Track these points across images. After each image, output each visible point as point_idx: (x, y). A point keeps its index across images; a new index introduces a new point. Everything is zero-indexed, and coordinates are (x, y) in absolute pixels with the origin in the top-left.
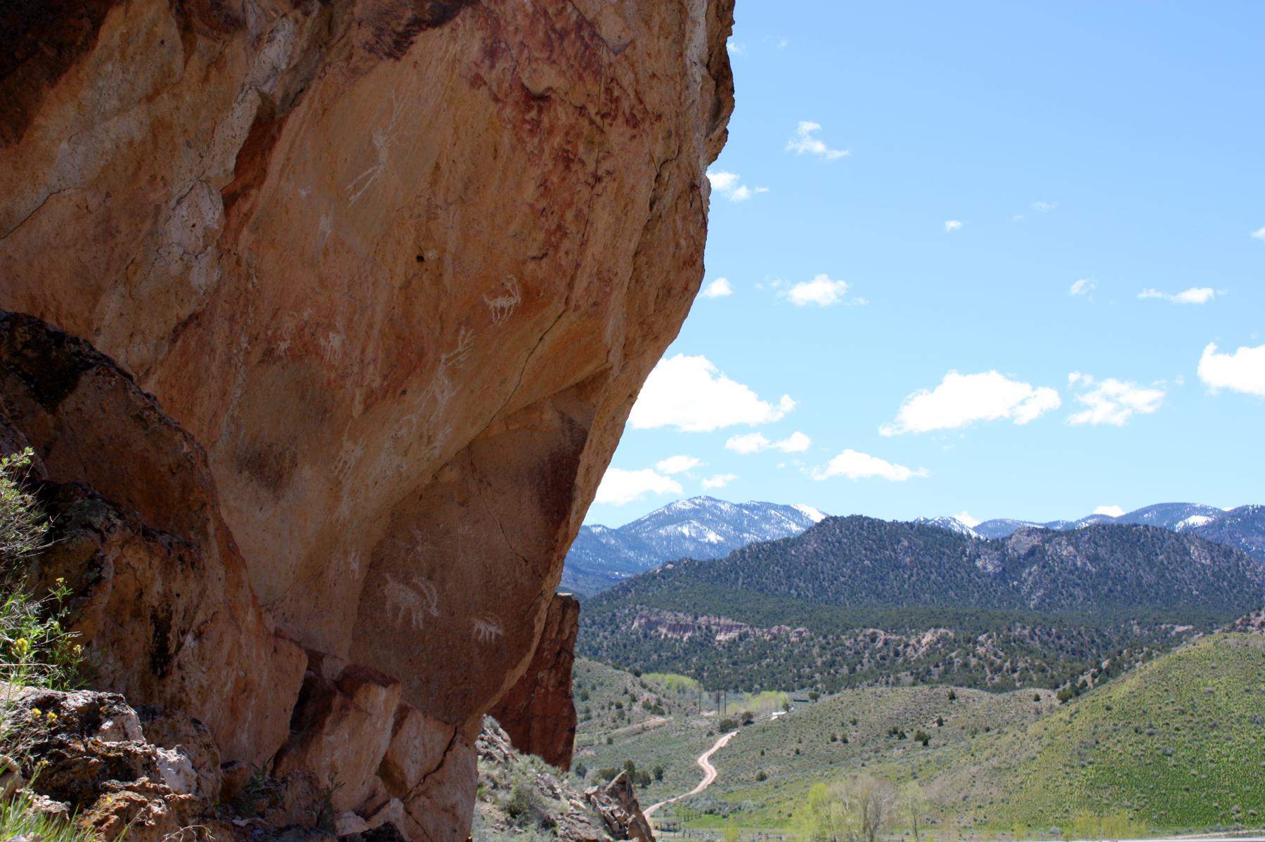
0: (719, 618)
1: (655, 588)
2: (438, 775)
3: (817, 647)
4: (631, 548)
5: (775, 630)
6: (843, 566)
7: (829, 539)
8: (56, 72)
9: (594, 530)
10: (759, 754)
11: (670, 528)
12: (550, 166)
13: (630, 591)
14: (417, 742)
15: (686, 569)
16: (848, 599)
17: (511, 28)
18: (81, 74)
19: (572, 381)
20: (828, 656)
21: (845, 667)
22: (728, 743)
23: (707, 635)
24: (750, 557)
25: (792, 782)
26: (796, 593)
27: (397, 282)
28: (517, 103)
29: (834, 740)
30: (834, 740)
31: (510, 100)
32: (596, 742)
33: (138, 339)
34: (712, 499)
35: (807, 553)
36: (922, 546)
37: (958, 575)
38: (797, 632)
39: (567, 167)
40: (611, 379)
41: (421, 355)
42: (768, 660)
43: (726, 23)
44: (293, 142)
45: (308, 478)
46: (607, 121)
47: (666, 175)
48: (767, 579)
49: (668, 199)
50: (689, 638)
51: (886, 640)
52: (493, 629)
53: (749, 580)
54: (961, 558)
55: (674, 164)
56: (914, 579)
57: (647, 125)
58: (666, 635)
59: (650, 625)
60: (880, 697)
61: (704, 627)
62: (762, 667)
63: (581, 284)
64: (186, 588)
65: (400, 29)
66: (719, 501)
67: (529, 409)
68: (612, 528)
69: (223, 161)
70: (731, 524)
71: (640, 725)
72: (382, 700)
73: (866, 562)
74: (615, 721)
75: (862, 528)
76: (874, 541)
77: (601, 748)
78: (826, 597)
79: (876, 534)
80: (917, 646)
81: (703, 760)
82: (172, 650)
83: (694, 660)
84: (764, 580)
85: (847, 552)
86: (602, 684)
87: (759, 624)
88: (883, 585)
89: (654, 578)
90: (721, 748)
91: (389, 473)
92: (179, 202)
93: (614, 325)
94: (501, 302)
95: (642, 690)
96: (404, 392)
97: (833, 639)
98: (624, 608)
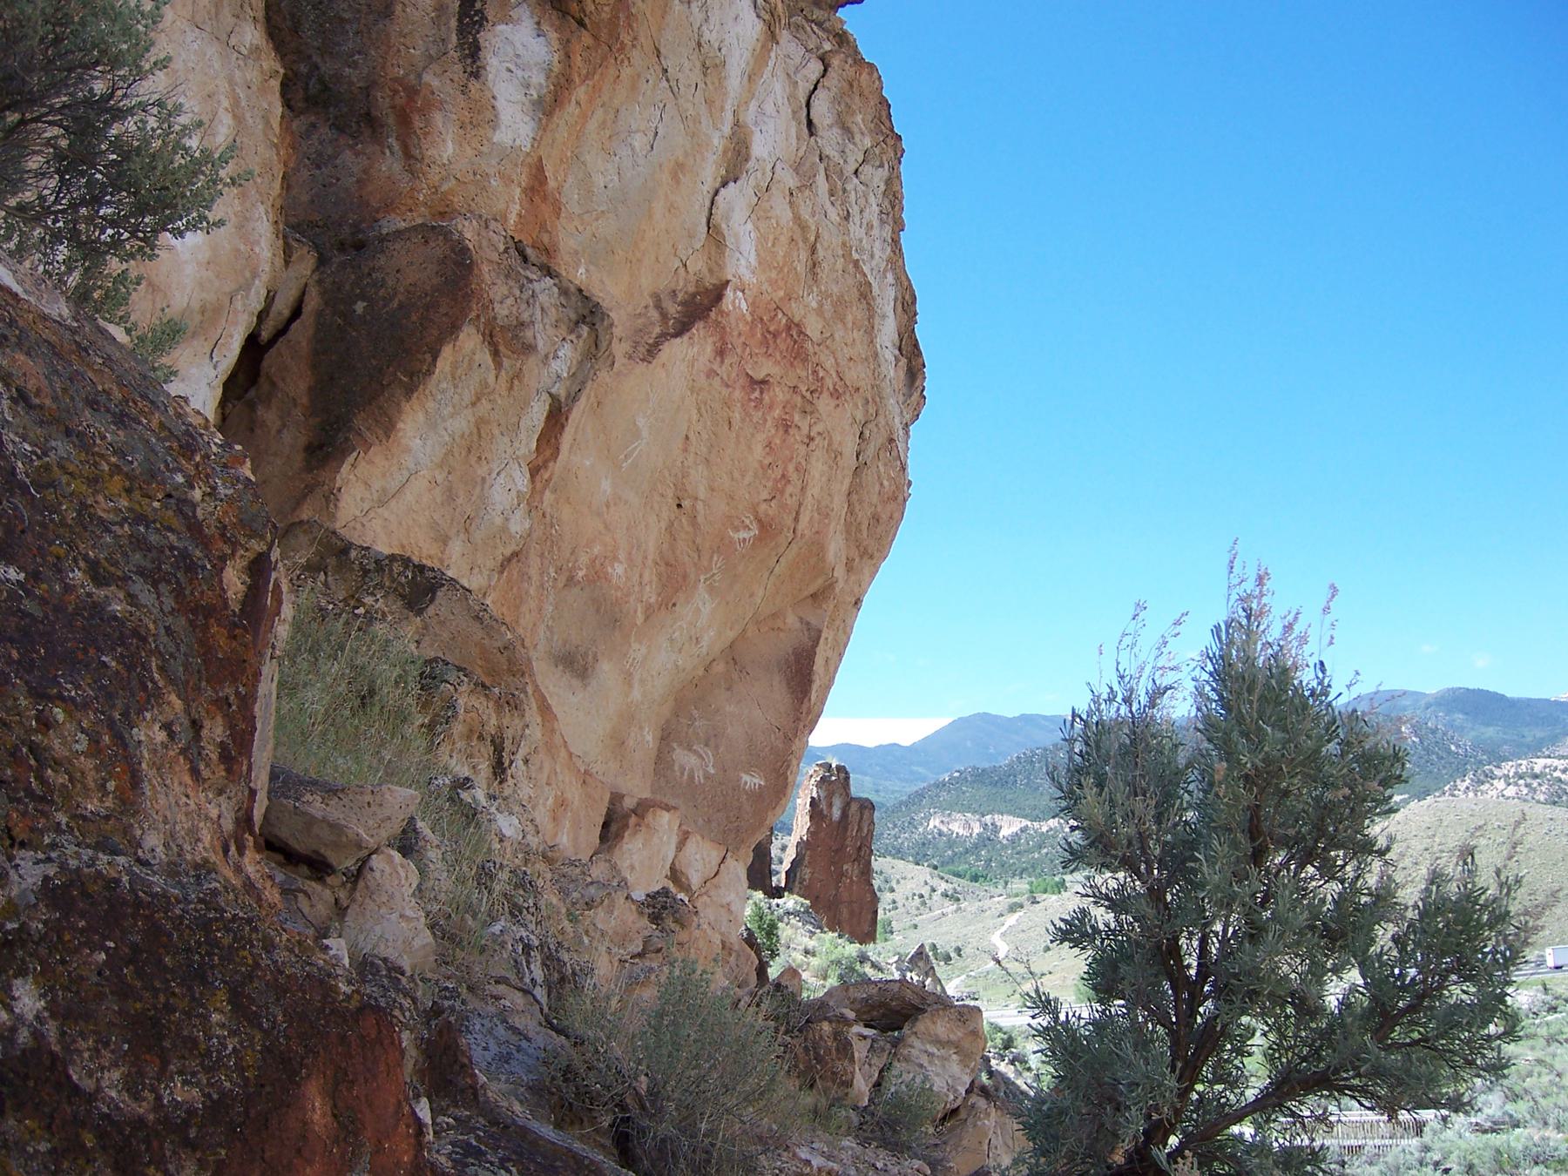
2: (715, 881)
8: (410, 390)
12: (773, 431)
14: (698, 857)
17: (735, 333)
18: (427, 392)
19: (806, 593)
27: (663, 525)
28: (743, 387)
31: (738, 385)
33: (476, 570)
39: (786, 431)
40: (837, 590)
41: (685, 577)
43: (911, 314)
44: (577, 428)
45: (606, 670)
46: (816, 395)
47: (867, 433)
49: (870, 451)
52: (756, 781)
55: (874, 423)
57: (848, 396)
63: (804, 519)
64: (512, 724)
65: (651, 341)
67: (774, 616)
69: (527, 444)
72: (665, 823)
82: (506, 764)
91: (669, 666)
92: (498, 474)
93: (836, 548)
94: (743, 534)
96: (674, 605)
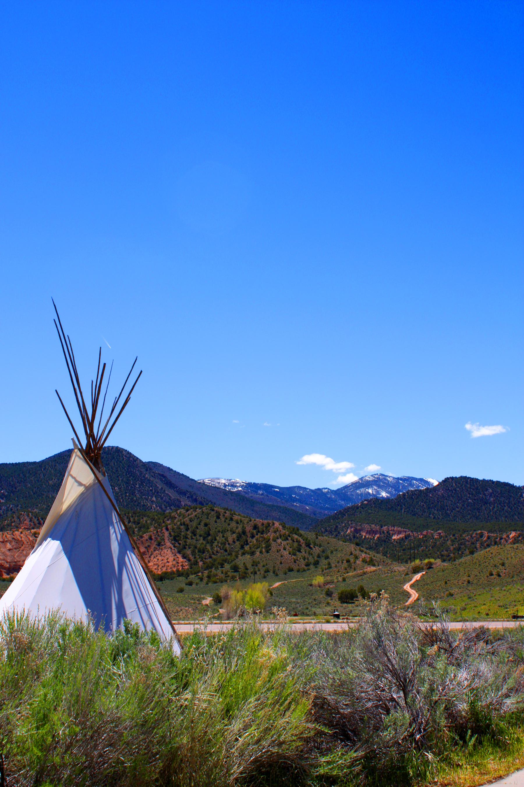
0: (394, 527)
1: (358, 513)
3: (449, 541)
4: (344, 500)
5: (425, 533)
6: (458, 503)
7: (450, 489)
9: (324, 490)
10: (444, 583)
11: (362, 490)
13: (345, 515)
15: (375, 504)
16: (460, 520)
20: (457, 545)
21: (467, 550)
22: (420, 578)
23: (387, 536)
24: (407, 498)
25: (480, 595)
26: (433, 517)
29: (491, 574)
30: (491, 574)
32: (336, 580)
34: (383, 475)
35: (438, 495)
36: (499, 492)
37: (519, 508)
38: (438, 533)
42: (422, 548)
48: (417, 509)
50: (378, 537)
51: (488, 536)
53: (408, 509)
54: (520, 499)
56: (495, 509)
58: (365, 536)
59: (357, 531)
60: (517, 549)
61: (386, 532)
62: (419, 551)
66: (387, 476)
68: (333, 489)
70: (393, 488)
71: (361, 571)
73: (469, 500)
74: (346, 569)
75: (467, 483)
76: (473, 489)
77: (338, 583)
78: (449, 519)
79: (474, 486)
80: (507, 538)
81: (407, 587)
83: (381, 549)
84: (416, 509)
85: (459, 495)
86: (336, 550)
87: (416, 530)
88: (479, 512)
89: (358, 508)
90: (417, 580)
95: (360, 553)
97: (458, 536)
98: (342, 523)
